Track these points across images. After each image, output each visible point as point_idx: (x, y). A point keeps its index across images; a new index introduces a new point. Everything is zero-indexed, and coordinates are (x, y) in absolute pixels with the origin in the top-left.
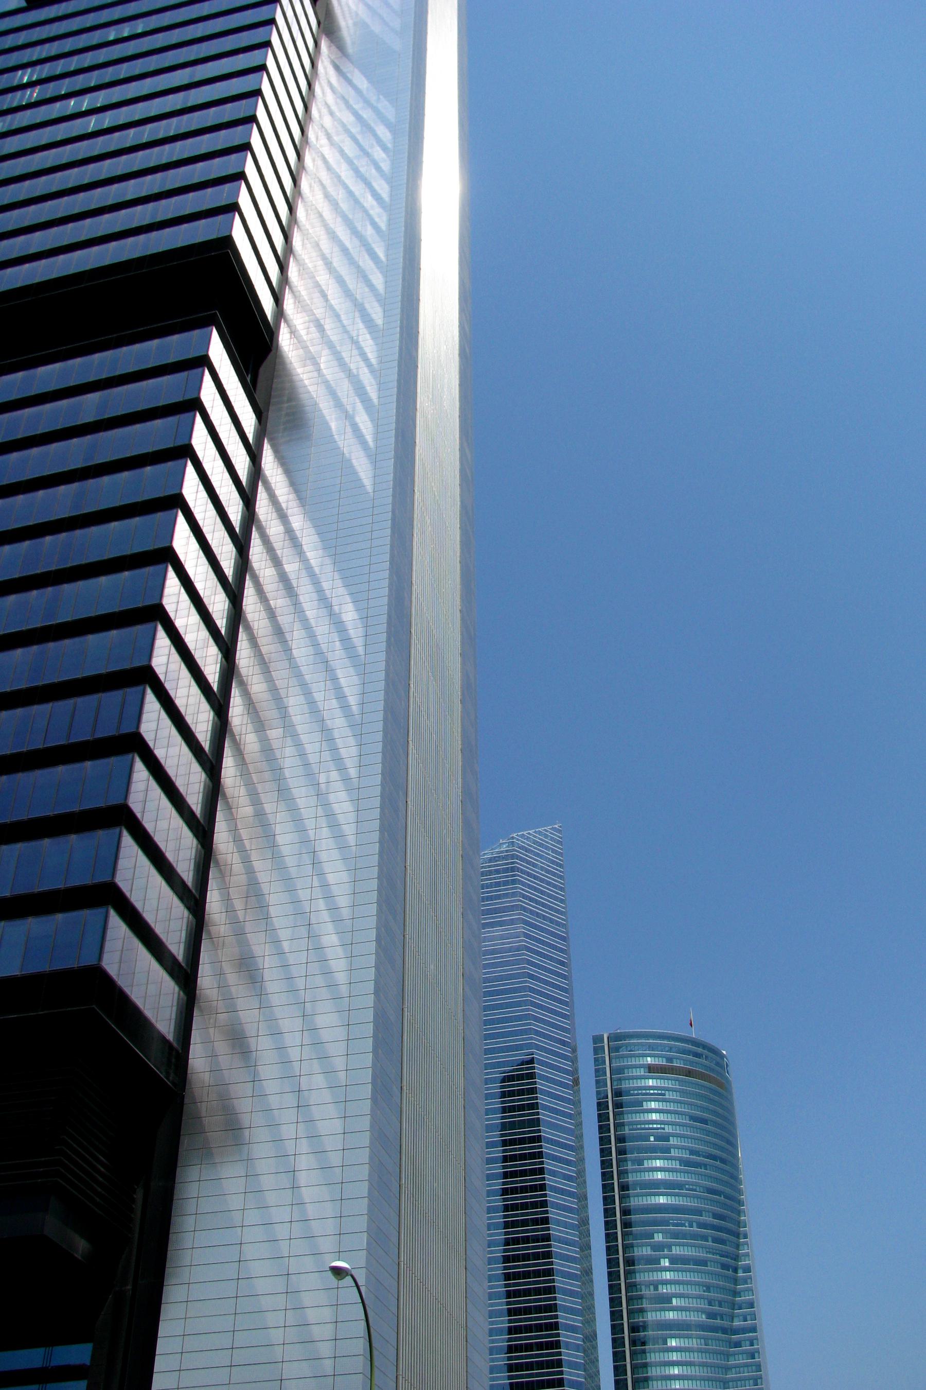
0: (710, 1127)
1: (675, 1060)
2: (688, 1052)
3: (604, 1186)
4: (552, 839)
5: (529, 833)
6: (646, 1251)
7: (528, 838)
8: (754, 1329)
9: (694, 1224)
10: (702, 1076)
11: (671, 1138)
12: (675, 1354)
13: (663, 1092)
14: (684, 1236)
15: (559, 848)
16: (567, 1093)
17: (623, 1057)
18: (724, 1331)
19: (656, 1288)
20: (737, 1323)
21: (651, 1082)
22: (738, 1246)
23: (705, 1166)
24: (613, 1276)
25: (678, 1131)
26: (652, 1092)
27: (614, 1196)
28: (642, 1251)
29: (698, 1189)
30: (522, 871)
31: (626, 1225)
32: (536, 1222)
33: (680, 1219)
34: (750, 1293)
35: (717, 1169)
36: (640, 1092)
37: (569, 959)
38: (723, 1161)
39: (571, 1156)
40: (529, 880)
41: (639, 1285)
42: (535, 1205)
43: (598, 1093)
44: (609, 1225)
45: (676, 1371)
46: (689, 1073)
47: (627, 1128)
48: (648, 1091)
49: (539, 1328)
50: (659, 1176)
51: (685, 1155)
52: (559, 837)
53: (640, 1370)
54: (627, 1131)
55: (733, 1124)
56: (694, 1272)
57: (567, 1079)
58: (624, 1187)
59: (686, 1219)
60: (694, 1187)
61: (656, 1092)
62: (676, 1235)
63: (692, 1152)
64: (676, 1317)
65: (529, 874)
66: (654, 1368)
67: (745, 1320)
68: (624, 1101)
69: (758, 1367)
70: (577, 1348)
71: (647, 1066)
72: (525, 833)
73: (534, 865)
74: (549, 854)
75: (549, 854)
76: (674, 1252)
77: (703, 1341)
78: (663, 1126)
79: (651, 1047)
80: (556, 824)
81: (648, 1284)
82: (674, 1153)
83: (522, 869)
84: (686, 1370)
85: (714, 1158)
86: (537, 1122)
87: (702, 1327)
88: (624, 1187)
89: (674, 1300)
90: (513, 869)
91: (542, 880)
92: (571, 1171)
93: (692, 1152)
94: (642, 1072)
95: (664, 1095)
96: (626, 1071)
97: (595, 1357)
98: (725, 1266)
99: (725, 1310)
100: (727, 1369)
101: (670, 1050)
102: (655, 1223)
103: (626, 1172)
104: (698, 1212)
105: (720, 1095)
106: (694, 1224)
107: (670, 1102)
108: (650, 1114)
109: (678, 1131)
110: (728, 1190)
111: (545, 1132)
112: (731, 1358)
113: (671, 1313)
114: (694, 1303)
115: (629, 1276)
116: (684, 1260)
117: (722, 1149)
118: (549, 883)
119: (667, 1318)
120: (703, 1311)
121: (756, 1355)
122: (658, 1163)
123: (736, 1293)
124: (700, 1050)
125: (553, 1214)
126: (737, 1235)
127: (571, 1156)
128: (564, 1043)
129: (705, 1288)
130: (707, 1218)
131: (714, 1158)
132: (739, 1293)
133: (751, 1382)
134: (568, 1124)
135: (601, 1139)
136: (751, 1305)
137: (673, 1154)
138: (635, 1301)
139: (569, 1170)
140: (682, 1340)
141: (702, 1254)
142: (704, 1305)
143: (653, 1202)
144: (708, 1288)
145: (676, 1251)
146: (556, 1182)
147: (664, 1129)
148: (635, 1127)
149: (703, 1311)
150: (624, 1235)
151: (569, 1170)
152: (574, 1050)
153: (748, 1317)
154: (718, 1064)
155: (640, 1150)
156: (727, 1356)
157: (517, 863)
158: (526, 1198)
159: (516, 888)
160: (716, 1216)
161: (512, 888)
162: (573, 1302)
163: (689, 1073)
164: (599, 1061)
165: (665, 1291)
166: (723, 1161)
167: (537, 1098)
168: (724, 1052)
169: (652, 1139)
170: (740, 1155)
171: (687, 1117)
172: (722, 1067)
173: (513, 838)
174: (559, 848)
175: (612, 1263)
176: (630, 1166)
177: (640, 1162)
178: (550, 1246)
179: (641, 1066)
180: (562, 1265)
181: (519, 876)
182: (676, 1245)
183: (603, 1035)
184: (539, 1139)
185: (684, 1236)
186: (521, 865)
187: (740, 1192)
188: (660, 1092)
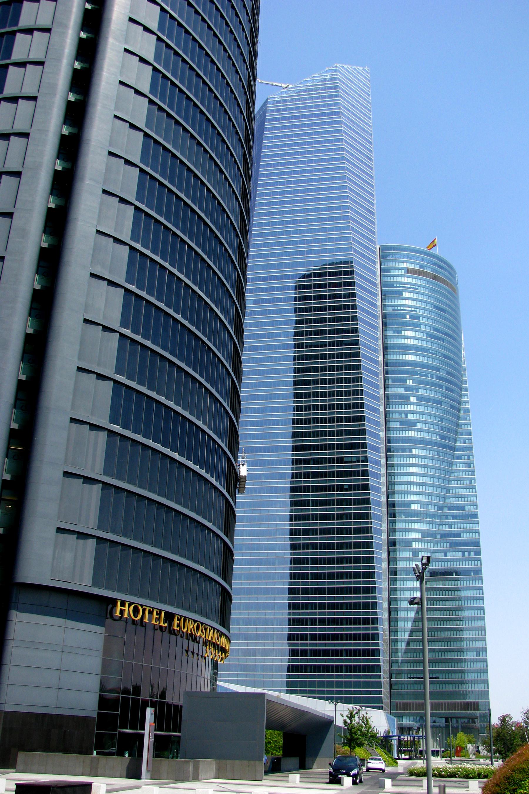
2: (435, 264)
5: (347, 67)
6: (401, 391)
8: (471, 449)
9: (434, 377)
14: (427, 383)
17: (390, 261)
19: (406, 416)
21: (405, 280)
22: (461, 396)
23: (443, 340)
33: (425, 372)
36: (401, 285)
59: (429, 373)
60: (435, 352)
62: (421, 382)
63: (435, 329)
67: (465, 443)
69: (473, 472)
71: (406, 269)
78: (416, 310)
79: (408, 257)
82: (422, 328)
90: (335, 88)
93: (435, 329)
94: (402, 272)
95: (418, 289)
98: (452, 407)
99: (452, 435)
101: (423, 260)
104: (438, 369)
106: (434, 377)
121: (472, 465)
126: (461, 389)
129: (439, 419)
130: (444, 375)
133: (468, 481)
136: (469, 434)
141: (439, 397)
144: (441, 420)
145: (421, 392)
147: (416, 311)
148: (396, 308)
153: (467, 441)
155: (399, 324)
161: (336, 92)
163: (435, 277)
169: (408, 317)
170: (463, 339)
173: (336, 66)
177: (399, 332)
179: (402, 269)
180: (367, 364)
182: (421, 389)
185: (427, 383)
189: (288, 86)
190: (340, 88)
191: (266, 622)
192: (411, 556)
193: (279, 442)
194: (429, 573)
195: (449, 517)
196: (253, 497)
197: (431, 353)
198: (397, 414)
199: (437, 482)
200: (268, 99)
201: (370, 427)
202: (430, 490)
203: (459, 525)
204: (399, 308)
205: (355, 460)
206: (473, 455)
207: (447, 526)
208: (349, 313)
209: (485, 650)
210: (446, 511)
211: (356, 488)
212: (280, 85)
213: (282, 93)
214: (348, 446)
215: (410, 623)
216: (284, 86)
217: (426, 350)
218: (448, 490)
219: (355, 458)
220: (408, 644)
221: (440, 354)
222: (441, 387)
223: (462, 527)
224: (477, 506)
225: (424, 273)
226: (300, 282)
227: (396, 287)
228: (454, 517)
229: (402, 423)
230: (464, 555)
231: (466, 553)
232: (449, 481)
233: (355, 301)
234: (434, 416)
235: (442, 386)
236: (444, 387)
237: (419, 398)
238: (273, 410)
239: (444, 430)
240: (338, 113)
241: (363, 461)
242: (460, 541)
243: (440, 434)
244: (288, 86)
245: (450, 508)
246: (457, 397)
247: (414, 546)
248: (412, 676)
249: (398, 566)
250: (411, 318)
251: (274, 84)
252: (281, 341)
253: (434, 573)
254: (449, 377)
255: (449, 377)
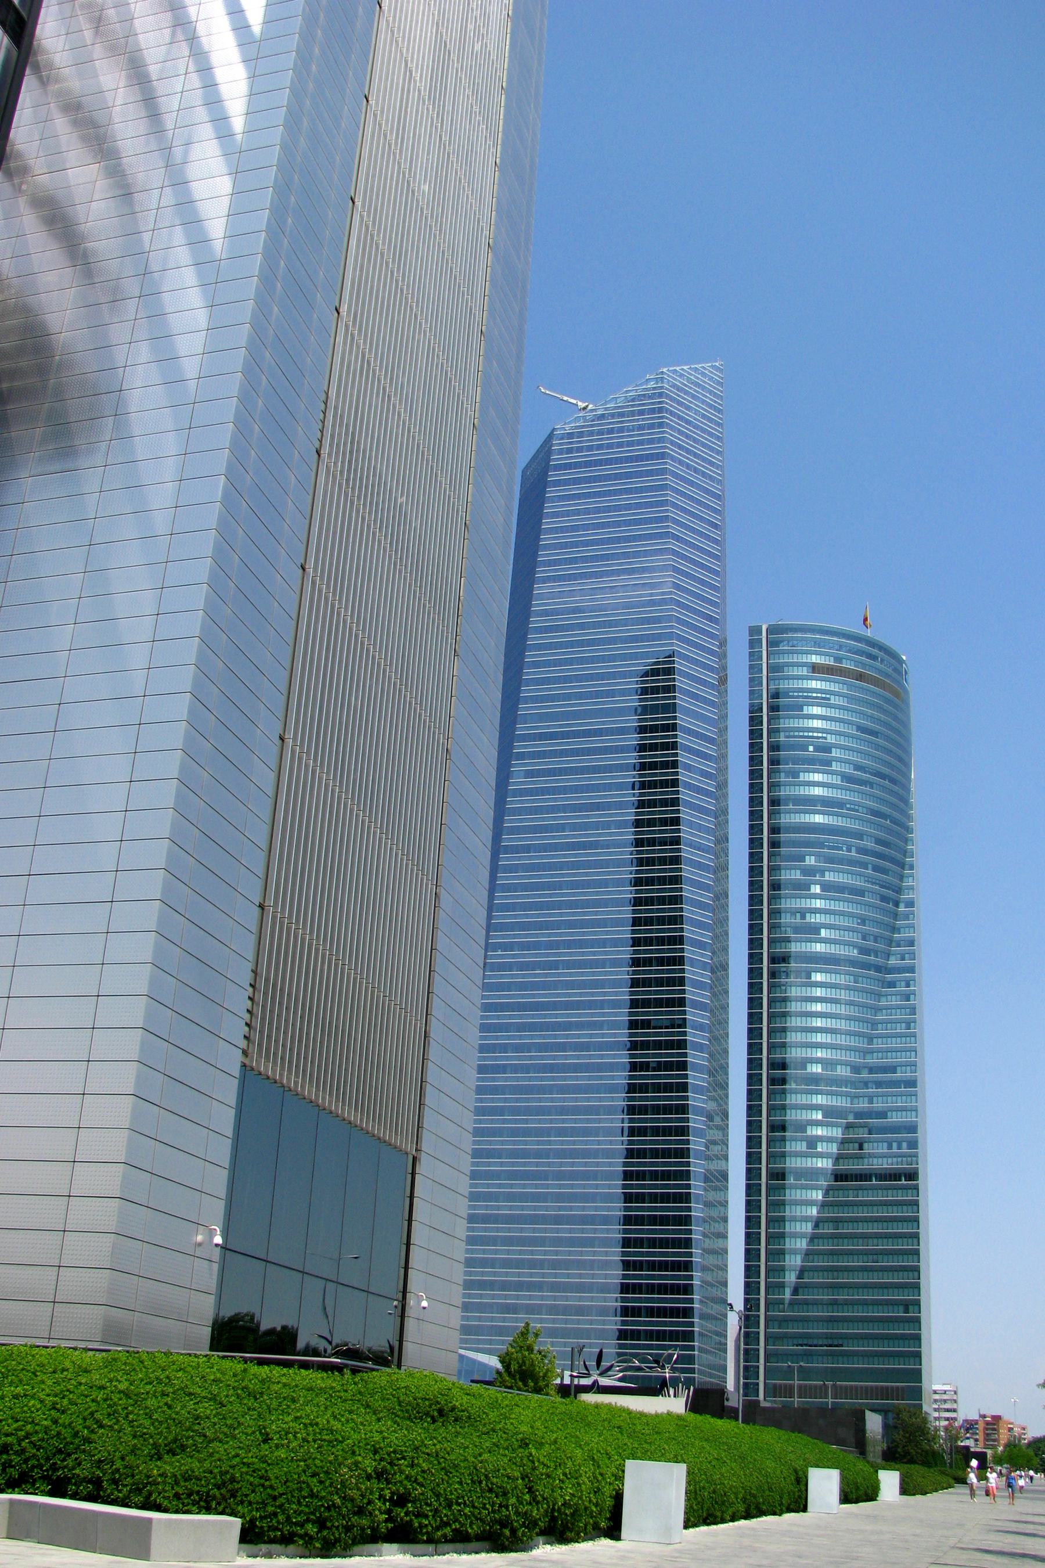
0: (880, 741)
1: (844, 661)
3: (751, 926)
4: (711, 379)
5: (682, 369)
6: (796, 875)
7: (681, 376)
8: (911, 969)
9: (853, 849)
10: (875, 682)
11: (833, 750)
12: (819, 989)
13: (828, 696)
14: (841, 861)
15: (719, 390)
16: (711, 695)
17: (784, 652)
18: (878, 969)
19: (803, 917)
20: (893, 961)
21: (814, 684)
22: (901, 878)
23: (871, 785)
24: (754, 900)
25: (842, 741)
26: (814, 695)
27: (762, 853)
28: (790, 875)
29: (861, 811)
30: (672, 413)
31: (774, 844)
32: (664, 822)
34: (912, 930)
35: (884, 788)
36: (801, 694)
37: (723, 520)
38: (893, 781)
39: (711, 750)
40: (680, 454)
41: (784, 985)
42: (664, 803)
43: (751, 705)
44: (755, 843)
45: (818, 1007)
46: (860, 677)
47: (782, 734)
48: (810, 694)
49: (661, 941)
50: (817, 791)
51: (848, 770)
52: (719, 377)
53: (778, 1050)
54: (782, 738)
55: (908, 741)
56: (849, 945)
57: (712, 678)
58: (774, 802)
59: (844, 843)
60: (857, 807)
61: (819, 695)
62: (830, 860)
63: (858, 767)
64: (823, 950)
65: (680, 418)
66: (793, 1049)
67: (903, 959)
68: (781, 704)
69: (913, 1010)
70: (704, 966)
72: (678, 369)
73: (688, 408)
74: (706, 397)
75: (706, 397)
76: (827, 878)
77: (852, 978)
78: (824, 735)
79: (817, 643)
80: (716, 362)
81: (794, 912)
82: (835, 766)
83: (671, 411)
84: (829, 1023)
85: (882, 776)
86: (673, 708)
87: (853, 963)
88: (774, 802)
89: (823, 931)
91: (696, 427)
92: (710, 767)
94: (804, 671)
96: (786, 669)
97: (723, 1019)
98: (884, 899)
99: (881, 946)
100: (877, 1010)
101: (841, 647)
102: (808, 844)
103: (778, 868)
104: (859, 835)
105: (896, 706)
106: (853, 849)
107: (835, 708)
108: (813, 900)
109: (842, 741)
110: (896, 815)
111: (682, 720)
112: (883, 999)
113: (818, 945)
114: (847, 936)
115: (773, 1004)
116: (840, 888)
117: (892, 767)
118: (704, 431)
119: (813, 950)
120: (854, 945)
121: (912, 997)
122: (817, 777)
123: (894, 929)
124: (875, 651)
125: (685, 814)
126: (902, 865)
127: (711, 750)
128: (710, 618)
130: (869, 844)
131: (882, 776)
132: (899, 929)
133: (904, 1025)
134: (710, 713)
135: (751, 786)
136: (911, 943)
137: (834, 768)
138: (778, 1159)
139: (708, 766)
140: (828, 975)
141: (859, 883)
142: (856, 939)
143: (809, 1165)
144: (863, 921)
145: (829, 877)
146: (691, 778)
147: (825, 738)
148: (792, 734)
149: (854, 945)
150: (770, 856)
151: (708, 766)
152: (723, 643)
154: (895, 670)
155: (796, 761)
156: (879, 995)
157: (667, 403)
158: (656, 775)
159: (663, 432)
160: (879, 841)
161: (660, 418)
162: (702, 915)
163: (860, 677)
164: (754, 656)
165: (813, 920)
166: (893, 781)
167: (674, 680)
168: (904, 658)
169: (811, 748)
170: (912, 777)
171: (854, 727)
172: (900, 673)
173: (662, 373)
174: (719, 390)
175: (754, 885)
176: (783, 778)
177: (795, 774)
178: (679, 850)
180: (693, 873)
181: (667, 403)
182: (829, 871)
183: (761, 626)
184: (674, 727)
185: (841, 861)
186: (671, 406)
187: (909, 818)
188: (824, 696)
189: (587, 406)
190: (667, 410)
191: (533, 1264)
192: (804, 1149)
193: (558, 995)
194: (833, 1177)
195: (870, 1085)
196: (518, 1079)
197: (848, 809)
198: (788, 915)
199: (853, 1027)
200: (554, 429)
201: (694, 973)
202: (841, 1040)
203: (885, 1098)
204: (796, 734)
205: (668, 1023)
206: (914, 980)
207: (866, 1099)
208: (667, 793)
209: (917, 1303)
210: (865, 1075)
211: (669, 1066)
212: (574, 401)
213: (577, 419)
214: (659, 1003)
215: (799, 1258)
216: (581, 405)
217: (840, 804)
218: (870, 1040)
219: (669, 1021)
220: (795, 1291)
221: (865, 809)
222: (865, 865)
223: (891, 1103)
224: (916, 1066)
225: (841, 670)
226: (643, 682)
227: (793, 697)
228: (879, 1084)
229: (797, 929)
230: (890, 1147)
231: (895, 1145)
232: (872, 1024)
233: (677, 773)
234: (851, 915)
235: (867, 864)
236: (870, 866)
237: (826, 887)
238: (551, 945)
239: (867, 939)
240: (663, 456)
241: (679, 1026)
242: (885, 1125)
243: (860, 945)
244: (587, 406)
245: (871, 1070)
246: (895, 881)
247: (809, 1133)
248: (800, 1342)
249: (788, 1165)
250: (816, 749)
251: (565, 398)
252: (567, 837)
253: (841, 1175)
254: (879, 848)
255: (879, 848)
